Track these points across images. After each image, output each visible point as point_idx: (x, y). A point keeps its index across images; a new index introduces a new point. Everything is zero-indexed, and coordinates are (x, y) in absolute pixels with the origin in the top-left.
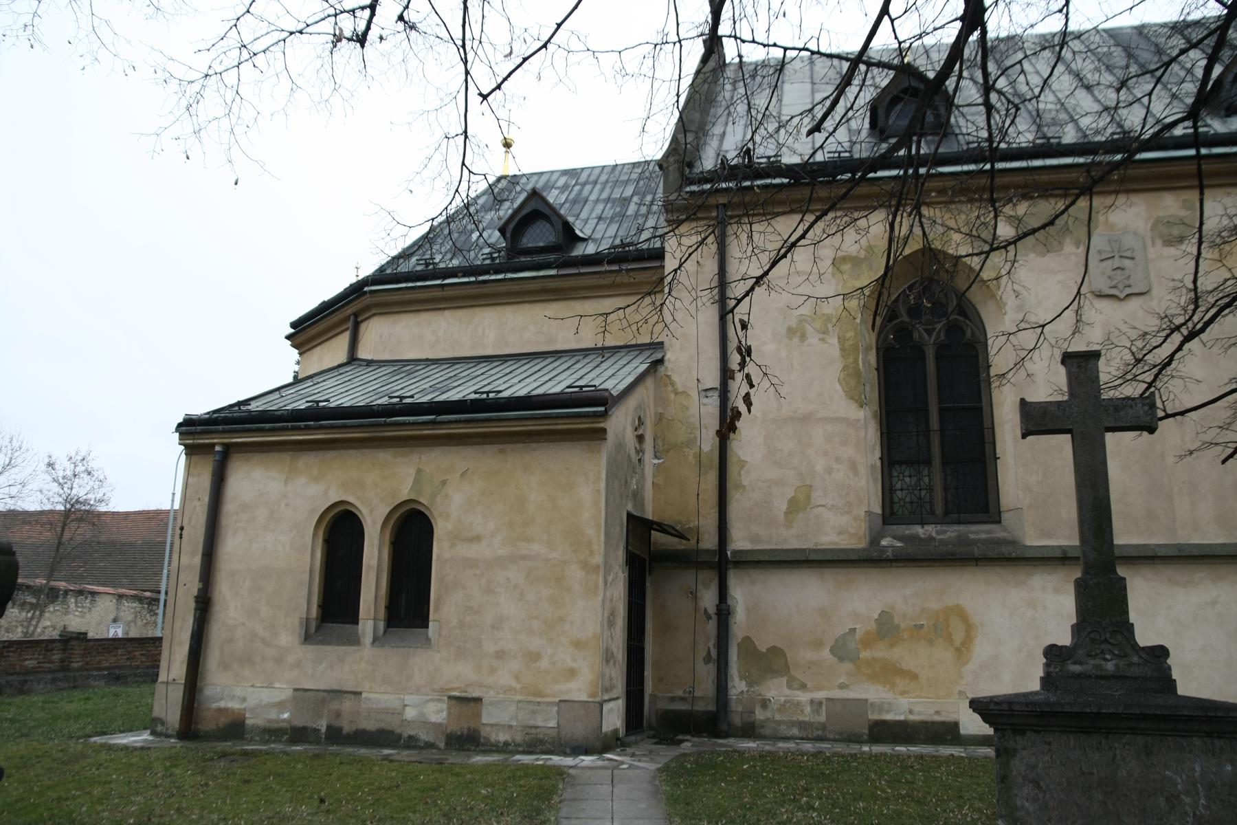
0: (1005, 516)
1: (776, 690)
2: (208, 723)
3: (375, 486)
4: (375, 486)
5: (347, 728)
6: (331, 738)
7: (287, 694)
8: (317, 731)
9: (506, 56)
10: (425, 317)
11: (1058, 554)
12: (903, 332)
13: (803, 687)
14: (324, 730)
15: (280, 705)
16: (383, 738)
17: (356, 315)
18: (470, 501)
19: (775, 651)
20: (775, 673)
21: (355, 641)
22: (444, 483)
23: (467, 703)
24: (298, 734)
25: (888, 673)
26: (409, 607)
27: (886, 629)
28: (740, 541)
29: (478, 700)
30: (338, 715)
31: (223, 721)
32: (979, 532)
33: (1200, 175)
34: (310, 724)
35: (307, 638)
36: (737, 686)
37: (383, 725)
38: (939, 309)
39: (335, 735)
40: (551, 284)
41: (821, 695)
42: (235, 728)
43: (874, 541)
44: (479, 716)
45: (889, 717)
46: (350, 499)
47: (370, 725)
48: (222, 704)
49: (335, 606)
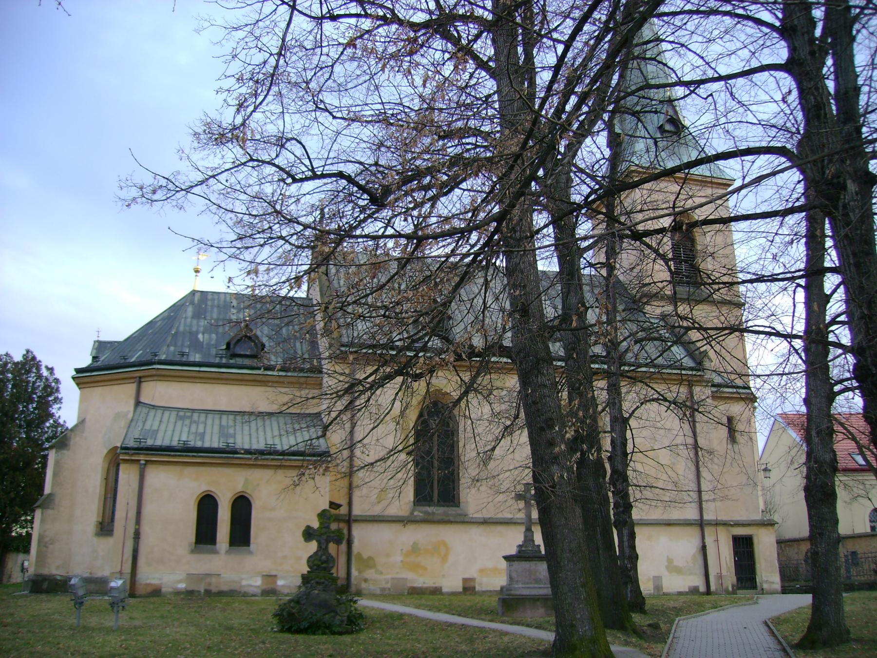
0: (461, 505)
1: (370, 574)
2: (140, 590)
3: (226, 484)
4: (226, 484)
5: (214, 589)
6: (203, 597)
7: (183, 576)
8: (199, 591)
9: (670, 561)
10: (186, 385)
11: (482, 520)
12: (425, 422)
13: (382, 573)
14: (202, 591)
15: (180, 581)
16: (232, 594)
17: (140, 377)
18: (266, 489)
19: (370, 558)
20: (371, 567)
21: (216, 552)
22: (258, 485)
23: (271, 577)
24: (190, 593)
25: (416, 567)
26: (241, 536)
27: (415, 549)
28: (357, 511)
29: (275, 576)
30: (210, 584)
31: (149, 589)
32: (452, 510)
33: (625, 523)
34: (196, 588)
35: (414, 543)
36: (354, 573)
37: (232, 588)
38: (437, 413)
39: (208, 592)
40: (259, 378)
41: (389, 576)
42: (156, 592)
43: (412, 513)
44: (275, 582)
45: (415, 585)
46: (213, 490)
47: (225, 588)
48: (148, 582)
49: (205, 534)
